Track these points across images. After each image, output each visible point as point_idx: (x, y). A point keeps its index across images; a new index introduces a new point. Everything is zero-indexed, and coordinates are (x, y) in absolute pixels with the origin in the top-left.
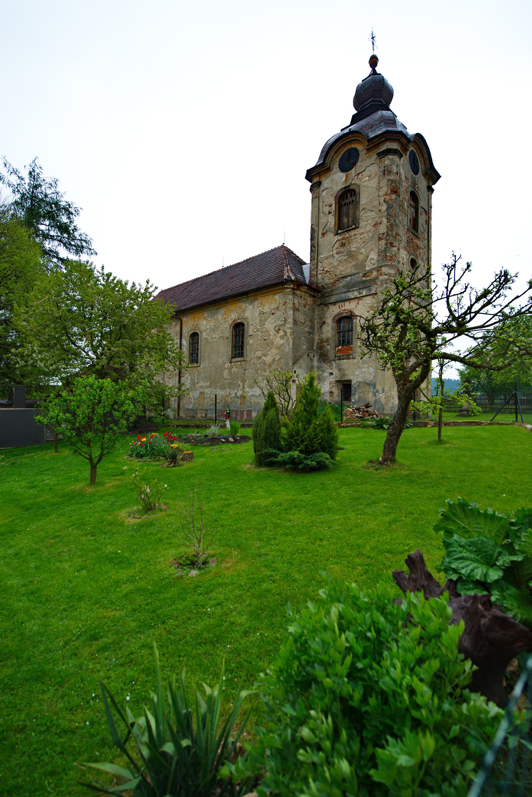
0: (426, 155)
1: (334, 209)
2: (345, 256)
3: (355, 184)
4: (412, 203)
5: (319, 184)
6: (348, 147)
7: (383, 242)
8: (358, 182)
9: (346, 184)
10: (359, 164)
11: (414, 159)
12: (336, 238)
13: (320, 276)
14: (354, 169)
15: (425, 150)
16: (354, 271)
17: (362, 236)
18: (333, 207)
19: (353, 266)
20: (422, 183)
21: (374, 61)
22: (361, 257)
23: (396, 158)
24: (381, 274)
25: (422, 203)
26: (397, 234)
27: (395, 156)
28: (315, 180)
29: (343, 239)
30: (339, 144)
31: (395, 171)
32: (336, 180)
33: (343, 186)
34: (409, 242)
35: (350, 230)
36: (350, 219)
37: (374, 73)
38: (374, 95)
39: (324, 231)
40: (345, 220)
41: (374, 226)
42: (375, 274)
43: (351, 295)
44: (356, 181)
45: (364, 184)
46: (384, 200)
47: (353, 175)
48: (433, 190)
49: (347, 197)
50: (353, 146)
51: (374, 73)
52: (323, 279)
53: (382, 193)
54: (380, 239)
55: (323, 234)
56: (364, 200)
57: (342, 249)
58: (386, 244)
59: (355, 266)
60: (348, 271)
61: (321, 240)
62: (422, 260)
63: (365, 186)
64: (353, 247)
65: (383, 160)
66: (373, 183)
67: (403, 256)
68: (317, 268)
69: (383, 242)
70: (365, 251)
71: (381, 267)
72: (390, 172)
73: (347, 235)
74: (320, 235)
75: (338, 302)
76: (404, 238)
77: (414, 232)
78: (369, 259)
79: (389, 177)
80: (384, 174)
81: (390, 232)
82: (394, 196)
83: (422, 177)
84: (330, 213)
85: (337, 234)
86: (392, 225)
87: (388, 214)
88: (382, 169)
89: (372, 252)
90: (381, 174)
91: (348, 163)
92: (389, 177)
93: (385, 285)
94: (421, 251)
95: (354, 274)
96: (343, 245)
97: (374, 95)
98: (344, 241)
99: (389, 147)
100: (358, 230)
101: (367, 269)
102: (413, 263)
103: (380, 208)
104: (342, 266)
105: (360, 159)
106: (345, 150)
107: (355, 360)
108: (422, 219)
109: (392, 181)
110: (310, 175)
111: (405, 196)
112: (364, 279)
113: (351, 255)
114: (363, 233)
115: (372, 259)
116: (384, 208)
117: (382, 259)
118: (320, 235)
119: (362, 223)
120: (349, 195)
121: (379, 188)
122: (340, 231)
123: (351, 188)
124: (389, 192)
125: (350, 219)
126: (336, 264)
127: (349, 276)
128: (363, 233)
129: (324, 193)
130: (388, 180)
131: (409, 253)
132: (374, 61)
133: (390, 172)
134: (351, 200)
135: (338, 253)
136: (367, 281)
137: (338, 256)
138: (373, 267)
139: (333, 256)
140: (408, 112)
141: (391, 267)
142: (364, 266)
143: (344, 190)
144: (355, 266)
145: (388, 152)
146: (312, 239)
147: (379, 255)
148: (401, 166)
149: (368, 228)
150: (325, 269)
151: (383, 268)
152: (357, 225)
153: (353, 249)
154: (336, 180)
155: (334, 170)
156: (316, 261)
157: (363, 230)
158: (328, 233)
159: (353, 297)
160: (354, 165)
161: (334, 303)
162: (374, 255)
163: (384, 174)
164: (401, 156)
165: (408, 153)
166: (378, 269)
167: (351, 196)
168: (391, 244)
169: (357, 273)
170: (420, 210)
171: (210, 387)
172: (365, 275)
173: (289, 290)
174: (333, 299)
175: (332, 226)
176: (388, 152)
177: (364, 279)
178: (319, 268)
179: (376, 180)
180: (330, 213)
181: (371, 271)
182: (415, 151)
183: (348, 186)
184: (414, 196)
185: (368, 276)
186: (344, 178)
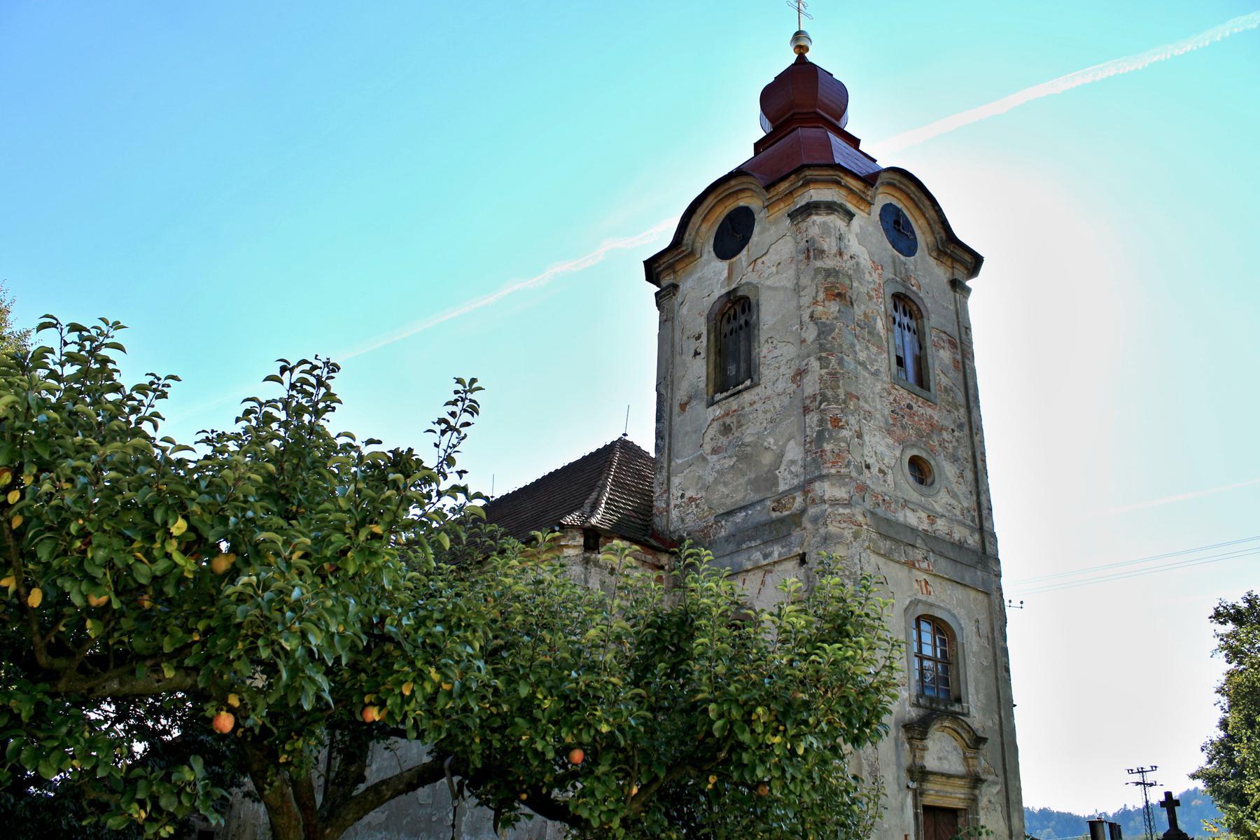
0: (931, 213)
1: (705, 344)
2: (731, 457)
3: (748, 284)
4: (906, 320)
5: (675, 287)
6: (731, 205)
7: (812, 419)
9: (729, 285)
10: (755, 238)
11: (897, 223)
13: (674, 513)
14: (744, 252)
15: (927, 203)
16: (752, 497)
18: (704, 339)
19: (750, 482)
20: (928, 273)
21: (801, 50)
22: (767, 459)
23: (836, 221)
25: (935, 320)
26: (849, 395)
27: (832, 217)
28: (666, 281)
30: (710, 200)
31: (834, 250)
32: (710, 277)
33: (724, 291)
34: (900, 414)
35: (740, 392)
37: (801, 60)
38: (802, 105)
40: (732, 370)
42: (799, 501)
44: (752, 277)
45: (768, 283)
46: (811, 317)
47: (744, 264)
48: (968, 290)
49: (735, 318)
50: (742, 203)
51: (801, 60)
52: (683, 520)
53: (806, 300)
54: (806, 410)
55: (683, 407)
56: (769, 314)
57: (723, 441)
58: (821, 422)
59: (755, 484)
60: (739, 497)
61: (677, 420)
62: (954, 459)
63: (769, 288)
65: (803, 225)
66: (786, 279)
67: (881, 449)
68: (668, 490)
69: (812, 419)
70: (776, 443)
71: (811, 482)
72: (823, 252)
73: (734, 404)
74: (676, 409)
76: (881, 408)
77: (917, 389)
78: (784, 463)
79: (819, 264)
80: (808, 257)
81: (829, 393)
82: (834, 307)
83: (933, 262)
84: (697, 354)
85: (711, 403)
86: (833, 375)
87: (822, 347)
88: (803, 244)
89: (792, 443)
90: (802, 257)
91: (734, 235)
92: (819, 264)
94: (945, 435)
95: (752, 505)
96: (726, 430)
97: (802, 105)
98: (728, 420)
99: (815, 198)
101: (782, 487)
102: (920, 470)
103: (804, 335)
104: (725, 484)
105: (756, 229)
106: (726, 212)
108: (941, 357)
109: (826, 270)
110: (653, 268)
111: (878, 310)
112: (774, 515)
113: (746, 456)
115: (793, 462)
116: (811, 334)
117: (814, 460)
118: (676, 409)
121: (798, 289)
122: (718, 396)
123: (740, 293)
124: (821, 296)
125: (743, 365)
126: (711, 479)
130: (817, 271)
131: (901, 442)
133: (821, 253)
134: (742, 322)
135: (715, 451)
136: (782, 520)
137: (715, 457)
138: (796, 482)
139: (704, 459)
140: (880, 130)
141: (840, 478)
142: (774, 482)
144: (755, 484)
145: (812, 208)
146: (659, 419)
147: (807, 452)
148: (859, 239)
149: (780, 386)
150: (688, 494)
151: (817, 485)
152: (755, 378)
153: (748, 439)
155: (705, 257)
156: (665, 473)
157: (769, 392)
158: (694, 403)
160: (745, 241)
162: (794, 451)
163: (808, 257)
164: (850, 216)
165: (876, 209)
166: (805, 487)
167: (743, 312)
168: (836, 422)
169: (761, 501)
170: (931, 337)
171: (386, 829)
175: (702, 385)
176: (812, 208)
177: (774, 515)
178: (673, 490)
179: (791, 272)
180: (697, 354)
182: (895, 202)
184: (904, 302)
186: (725, 274)
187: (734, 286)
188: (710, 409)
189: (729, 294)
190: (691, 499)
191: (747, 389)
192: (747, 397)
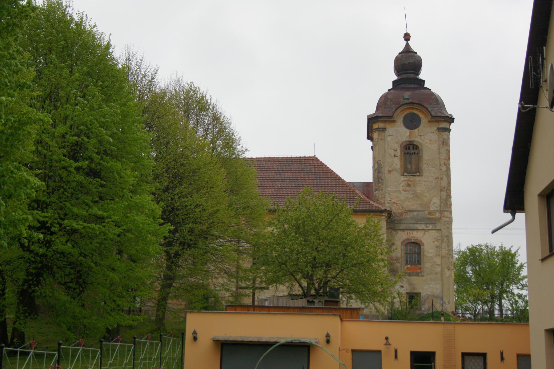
2: (411, 194)
8: (421, 142)
10: (421, 127)
12: (403, 178)
14: (416, 130)
17: (426, 183)
21: (407, 37)
24: (444, 216)
29: (409, 181)
33: (407, 139)
35: (415, 176)
36: (413, 167)
38: (408, 66)
39: (390, 169)
41: (436, 179)
43: (419, 226)
45: (426, 145)
46: (444, 163)
50: (415, 112)
54: (441, 190)
55: (390, 172)
57: (408, 188)
60: (414, 207)
64: (419, 189)
71: (444, 211)
75: (406, 230)
85: (403, 175)
90: (441, 143)
93: (447, 225)
97: (408, 66)
98: (410, 183)
100: (421, 177)
105: (422, 124)
107: (424, 278)
112: (429, 216)
113: (416, 196)
114: (426, 181)
115: (435, 203)
118: (387, 172)
119: (425, 174)
120: (411, 148)
122: (405, 174)
123: (415, 143)
127: (416, 211)
128: (426, 181)
129: (389, 138)
132: (407, 37)
135: (403, 190)
142: (429, 207)
143: (408, 143)
150: (393, 201)
151: (445, 212)
153: (418, 191)
154: (398, 133)
155: (399, 124)
159: (421, 228)
161: (403, 230)
163: (443, 144)
167: (413, 149)
172: (429, 214)
173: (384, 217)
174: (402, 226)
177: (429, 216)
180: (395, 156)
181: (435, 212)
183: (412, 141)
185: (432, 215)
186: (408, 134)
187: (412, 140)
188: (402, 177)
189: (410, 141)
190: (394, 203)
191: (418, 176)
192: (417, 178)
